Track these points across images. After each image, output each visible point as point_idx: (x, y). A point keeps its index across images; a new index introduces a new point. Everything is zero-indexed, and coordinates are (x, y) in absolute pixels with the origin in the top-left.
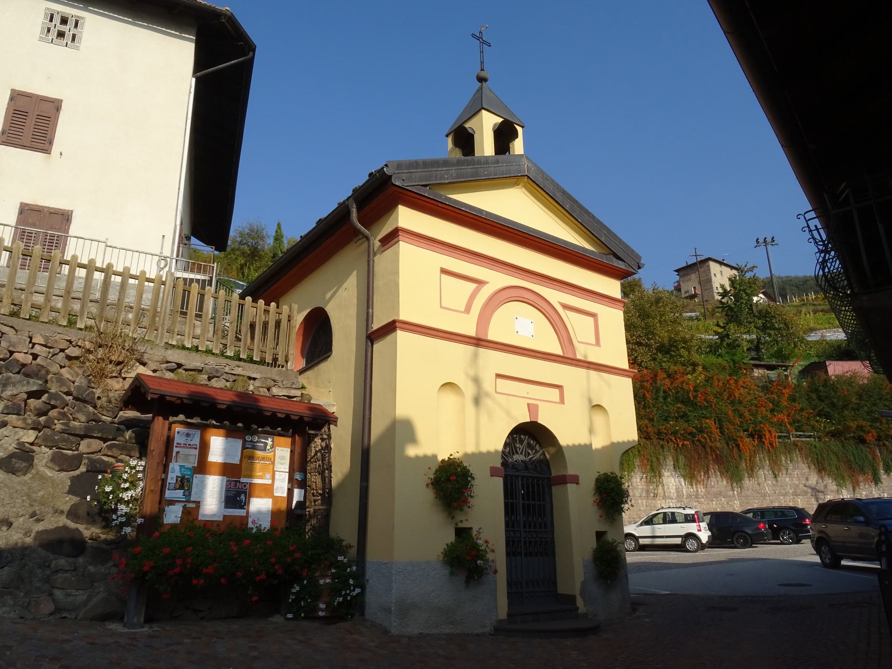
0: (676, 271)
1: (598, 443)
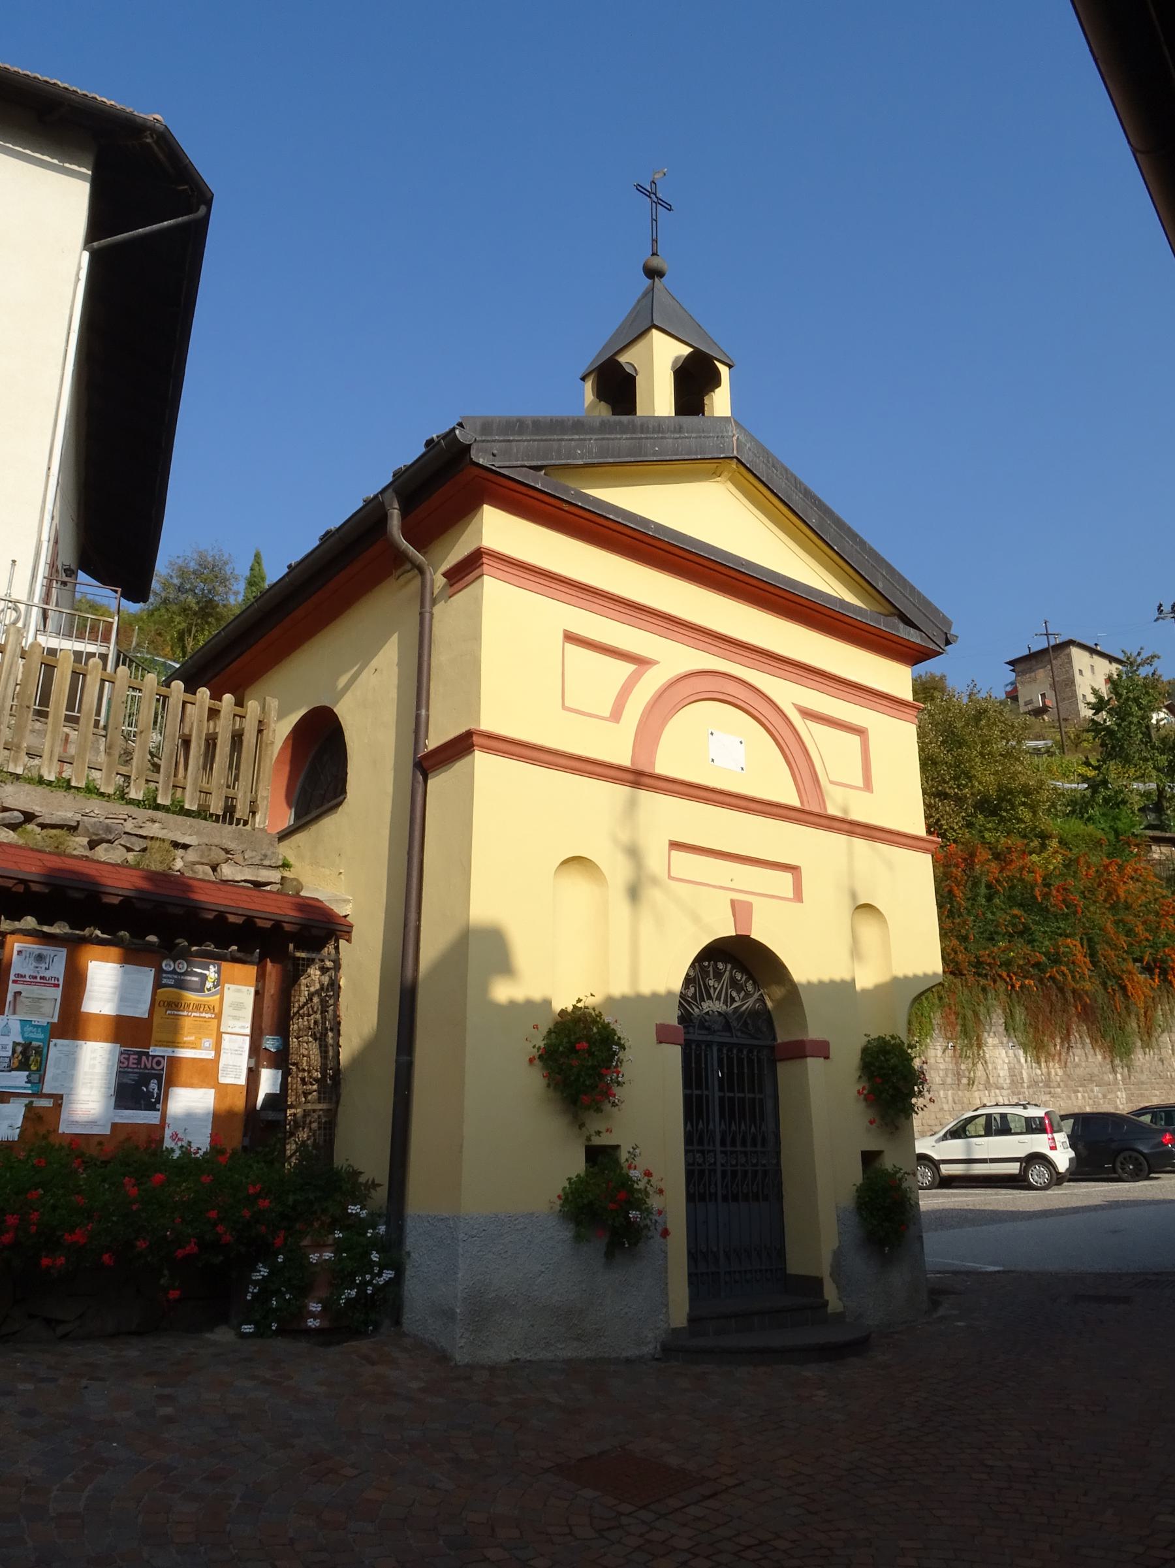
0: (1010, 663)
1: (867, 978)
